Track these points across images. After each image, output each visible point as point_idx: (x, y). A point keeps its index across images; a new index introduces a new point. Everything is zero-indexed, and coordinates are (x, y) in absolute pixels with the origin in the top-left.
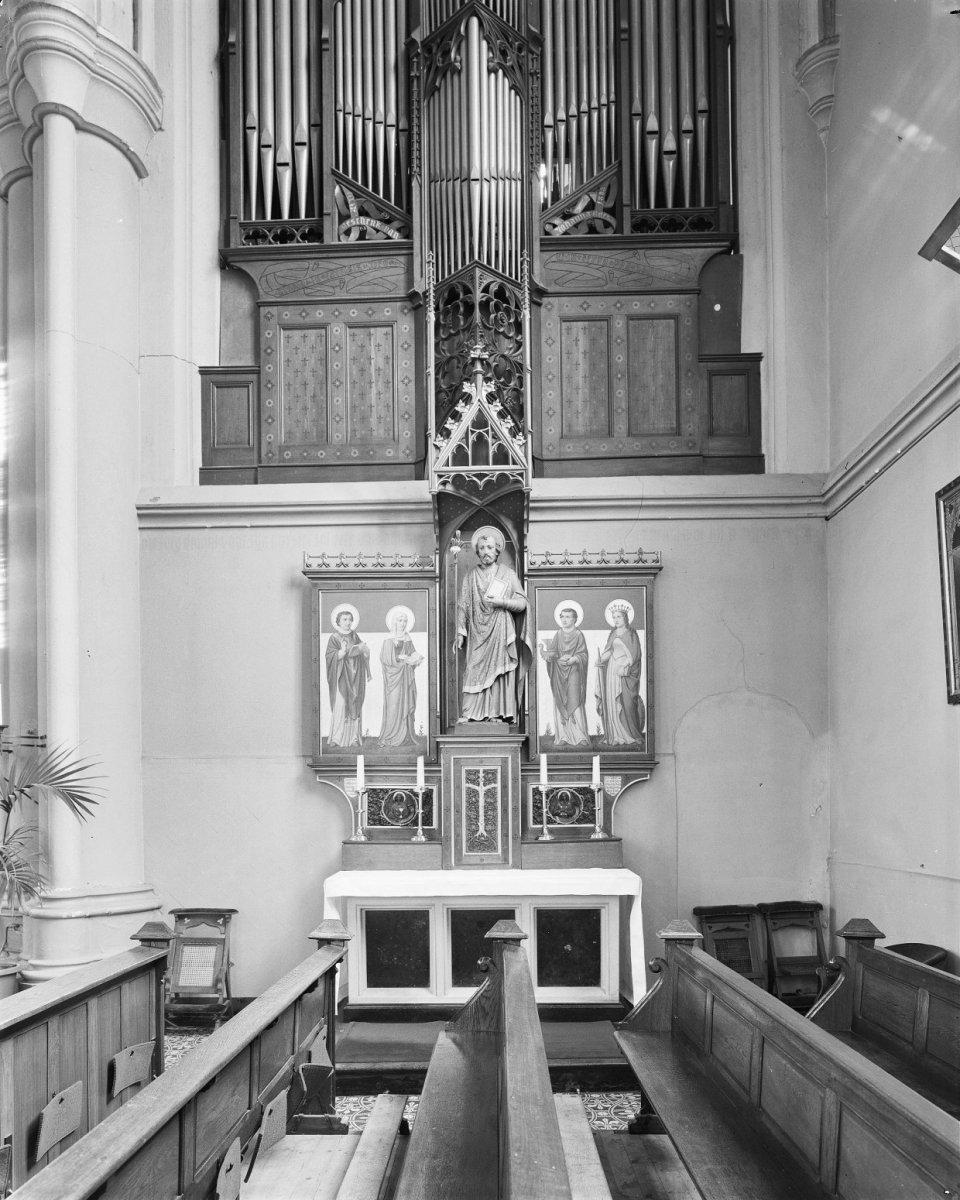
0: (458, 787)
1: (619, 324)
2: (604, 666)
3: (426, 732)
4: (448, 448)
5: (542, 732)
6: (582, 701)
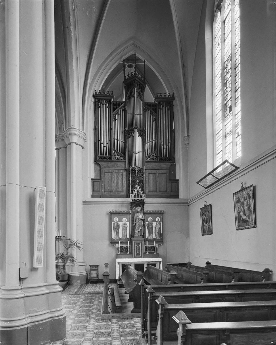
0: (134, 246)
1: (157, 174)
2: (156, 227)
3: (129, 237)
4: (133, 195)
5: (146, 237)
6: (152, 233)
